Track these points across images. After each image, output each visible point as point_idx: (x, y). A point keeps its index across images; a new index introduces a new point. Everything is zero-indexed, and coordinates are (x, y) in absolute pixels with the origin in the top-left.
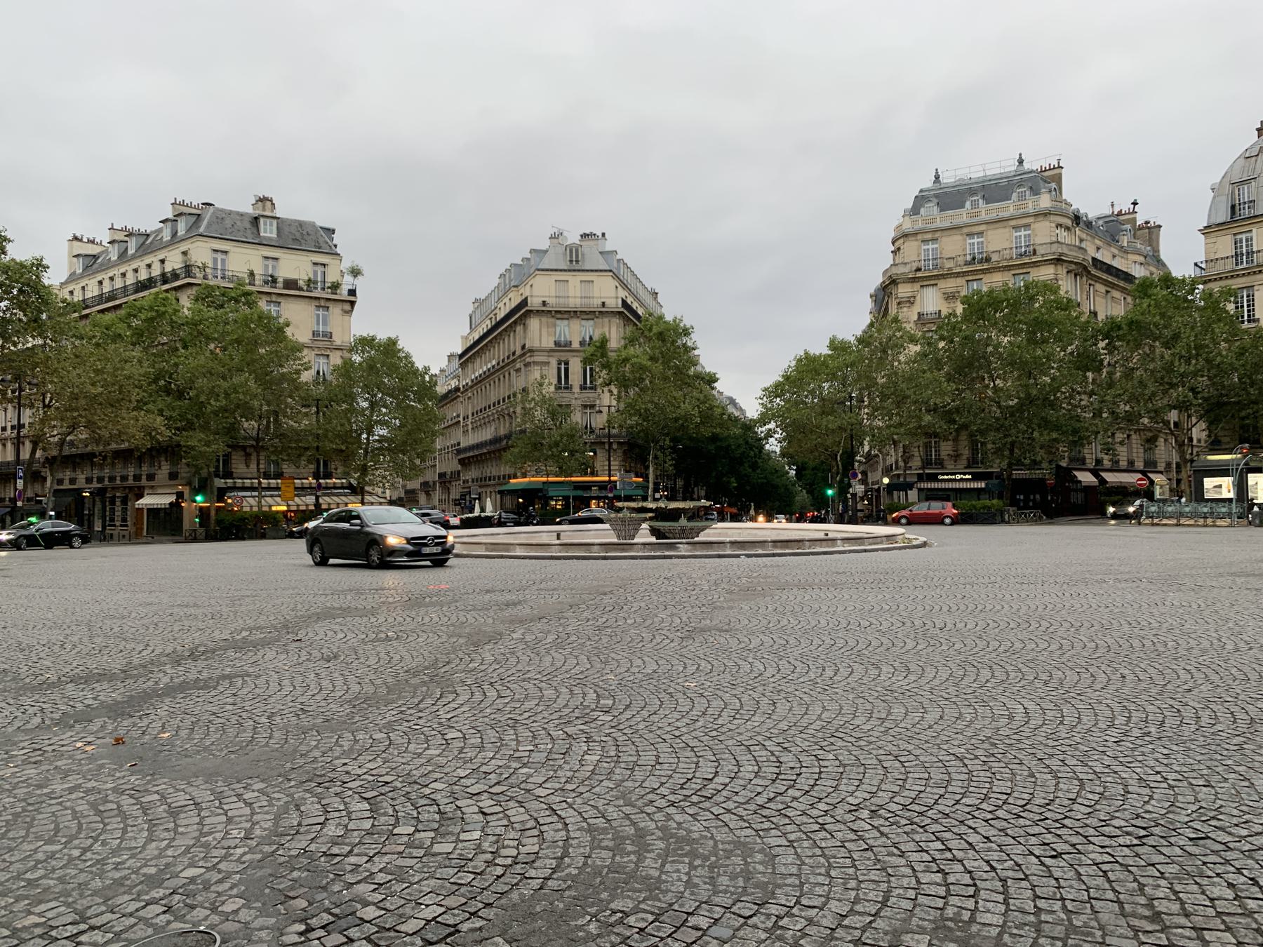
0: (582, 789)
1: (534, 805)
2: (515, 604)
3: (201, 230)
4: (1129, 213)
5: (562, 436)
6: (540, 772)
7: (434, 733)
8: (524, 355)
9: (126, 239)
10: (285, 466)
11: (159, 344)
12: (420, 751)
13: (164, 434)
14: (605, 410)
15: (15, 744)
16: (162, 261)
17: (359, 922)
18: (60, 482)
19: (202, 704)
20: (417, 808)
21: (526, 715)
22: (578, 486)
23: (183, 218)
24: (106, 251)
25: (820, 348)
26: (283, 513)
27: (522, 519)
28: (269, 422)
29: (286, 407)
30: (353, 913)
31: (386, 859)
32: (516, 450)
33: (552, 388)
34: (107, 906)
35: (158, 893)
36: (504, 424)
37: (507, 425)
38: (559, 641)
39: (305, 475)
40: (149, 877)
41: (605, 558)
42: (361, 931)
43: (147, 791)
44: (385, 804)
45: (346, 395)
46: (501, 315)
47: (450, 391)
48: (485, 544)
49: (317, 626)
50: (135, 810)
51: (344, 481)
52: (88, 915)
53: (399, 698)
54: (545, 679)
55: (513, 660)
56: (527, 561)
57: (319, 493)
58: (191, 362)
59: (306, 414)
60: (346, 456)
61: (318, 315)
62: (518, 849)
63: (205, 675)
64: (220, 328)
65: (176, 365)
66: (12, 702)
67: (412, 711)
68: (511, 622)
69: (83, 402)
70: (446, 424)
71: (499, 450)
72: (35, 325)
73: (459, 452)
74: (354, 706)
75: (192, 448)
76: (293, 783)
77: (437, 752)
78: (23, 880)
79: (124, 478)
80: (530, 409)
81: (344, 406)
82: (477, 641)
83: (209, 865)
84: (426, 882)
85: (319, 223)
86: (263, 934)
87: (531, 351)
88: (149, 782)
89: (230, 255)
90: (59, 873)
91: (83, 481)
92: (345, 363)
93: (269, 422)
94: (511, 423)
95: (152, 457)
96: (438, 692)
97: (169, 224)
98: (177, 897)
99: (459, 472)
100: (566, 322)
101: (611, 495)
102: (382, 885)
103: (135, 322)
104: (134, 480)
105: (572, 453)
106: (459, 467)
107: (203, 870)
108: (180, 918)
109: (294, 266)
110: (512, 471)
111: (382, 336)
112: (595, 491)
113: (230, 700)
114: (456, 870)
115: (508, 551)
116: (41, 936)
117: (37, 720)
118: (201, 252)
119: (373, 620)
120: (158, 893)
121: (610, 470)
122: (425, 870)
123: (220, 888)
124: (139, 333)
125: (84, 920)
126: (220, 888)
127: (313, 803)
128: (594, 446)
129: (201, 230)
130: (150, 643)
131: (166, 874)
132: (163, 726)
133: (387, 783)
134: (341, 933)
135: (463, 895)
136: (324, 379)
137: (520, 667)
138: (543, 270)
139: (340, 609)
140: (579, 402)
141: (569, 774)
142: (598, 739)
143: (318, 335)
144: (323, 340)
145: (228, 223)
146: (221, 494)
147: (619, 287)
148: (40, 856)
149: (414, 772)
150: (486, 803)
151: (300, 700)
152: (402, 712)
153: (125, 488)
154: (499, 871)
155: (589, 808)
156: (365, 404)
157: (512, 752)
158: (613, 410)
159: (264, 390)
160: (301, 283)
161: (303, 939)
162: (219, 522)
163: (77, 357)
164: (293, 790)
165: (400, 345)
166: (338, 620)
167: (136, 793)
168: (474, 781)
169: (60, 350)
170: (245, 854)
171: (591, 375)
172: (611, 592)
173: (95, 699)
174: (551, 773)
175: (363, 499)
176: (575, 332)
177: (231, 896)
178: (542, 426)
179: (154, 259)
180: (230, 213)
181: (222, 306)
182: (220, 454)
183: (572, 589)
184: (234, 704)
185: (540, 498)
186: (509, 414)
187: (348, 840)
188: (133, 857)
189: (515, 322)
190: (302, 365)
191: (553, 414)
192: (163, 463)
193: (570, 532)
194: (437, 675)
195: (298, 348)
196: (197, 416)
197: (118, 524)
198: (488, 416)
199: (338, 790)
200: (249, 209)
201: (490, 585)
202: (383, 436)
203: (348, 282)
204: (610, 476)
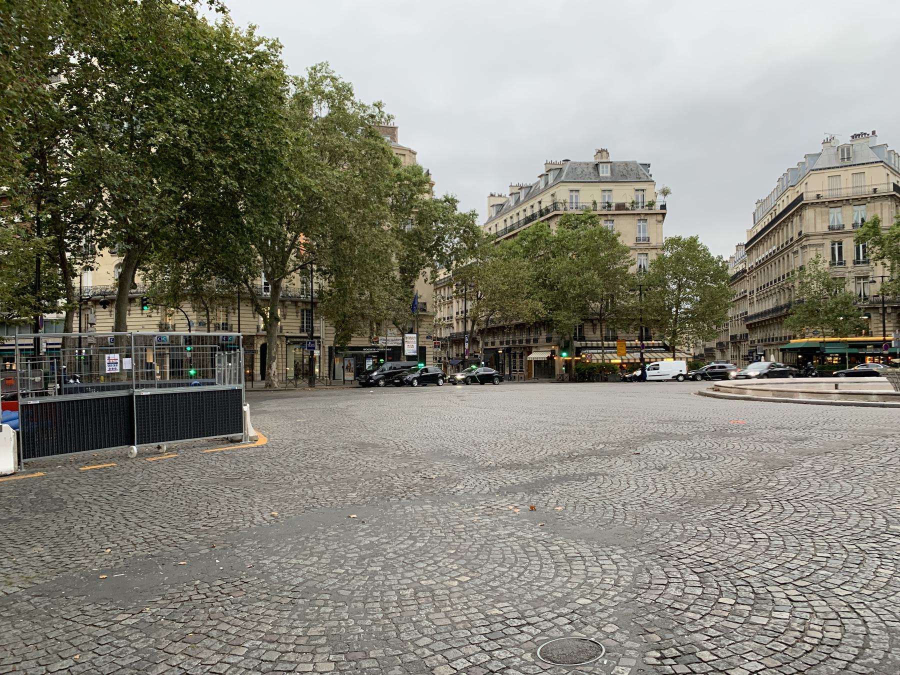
0: (877, 595)
1: (834, 601)
2: (802, 440)
3: (563, 178)
5: (837, 304)
6: (837, 576)
7: (744, 532)
8: (800, 239)
9: (519, 191)
10: (619, 332)
11: (539, 256)
12: (735, 544)
13: (543, 313)
14: (879, 280)
15: (477, 502)
16: (540, 202)
17: (698, 661)
18: (486, 344)
19: (580, 491)
20: (735, 586)
21: (821, 529)
22: (853, 345)
23: (552, 172)
24: (508, 201)
26: (621, 364)
27: (802, 372)
28: (607, 303)
29: (619, 292)
30: (694, 653)
31: (715, 619)
32: (795, 316)
33: (827, 265)
34: (535, 611)
35: (565, 610)
36: (784, 296)
37: (787, 296)
38: (846, 472)
39: (633, 338)
40: (558, 599)
41: (883, 406)
42: (701, 667)
43: (551, 543)
44: (710, 579)
45: (660, 281)
46: (780, 210)
47: (738, 273)
48: (772, 391)
49: (649, 445)
50: (546, 554)
51: (660, 342)
52: (526, 615)
53: (714, 503)
54: (835, 502)
55: (805, 484)
56: (810, 405)
57: (643, 351)
58: (558, 266)
59: (633, 296)
60: (661, 325)
61: (640, 226)
62: (822, 633)
63: (579, 472)
64: (575, 242)
65: (549, 268)
66: (473, 476)
67: (726, 514)
68: (801, 453)
69: (498, 295)
70: (736, 298)
71: (780, 317)
72: (472, 251)
73: (747, 319)
74: (682, 505)
75: (560, 322)
76: (643, 553)
77: (748, 547)
78: (489, 586)
79: (521, 341)
80: (807, 283)
81: (659, 289)
82: (773, 466)
83: (594, 599)
84: (746, 643)
85: (639, 161)
86: (632, 653)
87: (806, 236)
88: (552, 538)
89: (581, 192)
90: (507, 586)
91: (498, 343)
92: (659, 258)
93: (607, 303)
94: (790, 295)
95: (536, 328)
96: (745, 502)
97: (543, 177)
98: (576, 616)
99: (747, 335)
101: (886, 352)
102: (713, 637)
103: (525, 243)
105: (847, 318)
106: (747, 331)
107: (590, 601)
108: (579, 630)
109: (623, 194)
110: (792, 333)
111: (686, 236)
112: (870, 349)
113: (597, 490)
114: (772, 639)
115: (792, 397)
116: (501, 622)
117: (487, 489)
118: (563, 193)
119: (689, 443)
120: (565, 610)
121: (884, 331)
122: (746, 634)
123: (602, 615)
124: (527, 250)
125: (524, 618)
126: (602, 615)
127: (658, 569)
128: (868, 311)
129: (563, 178)
130: (544, 447)
131: (568, 599)
132: (557, 502)
133: (711, 564)
134: (686, 665)
135: (778, 659)
136: (645, 271)
137: (811, 490)
138: (817, 170)
139: (664, 433)
140: (853, 275)
141: (865, 581)
142: (890, 557)
143: (640, 240)
144: (643, 243)
145: (579, 171)
146: (578, 351)
147: (891, 175)
148: (496, 573)
149: (731, 559)
150: (792, 592)
151: (643, 495)
152: (717, 513)
154: (808, 647)
155: (886, 612)
156: (675, 287)
157: (811, 556)
158: (886, 279)
159: (604, 281)
160: (628, 205)
161: (659, 663)
162: (577, 370)
163: (494, 268)
164: (644, 558)
165: (700, 241)
166: (664, 442)
167: (547, 544)
168: (780, 574)
169: (485, 265)
170: (615, 596)
171: (864, 252)
172: (893, 435)
173: (517, 479)
174: (848, 578)
175: (674, 355)
176: (847, 217)
177: (609, 623)
178: (818, 297)
179: (534, 202)
180: (580, 164)
181: (576, 227)
182: (577, 325)
183: (854, 431)
184: (599, 493)
185: (818, 355)
186: (788, 288)
187: (685, 600)
188: (547, 584)
189: (792, 215)
190: (629, 262)
191: (828, 287)
192: (543, 332)
193: (847, 384)
194: (742, 489)
195: (626, 250)
196: (562, 301)
197: (518, 370)
198: (770, 290)
199: (676, 563)
200: (593, 160)
201: (779, 424)
202: (687, 309)
203: (660, 200)
204: (884, 335)
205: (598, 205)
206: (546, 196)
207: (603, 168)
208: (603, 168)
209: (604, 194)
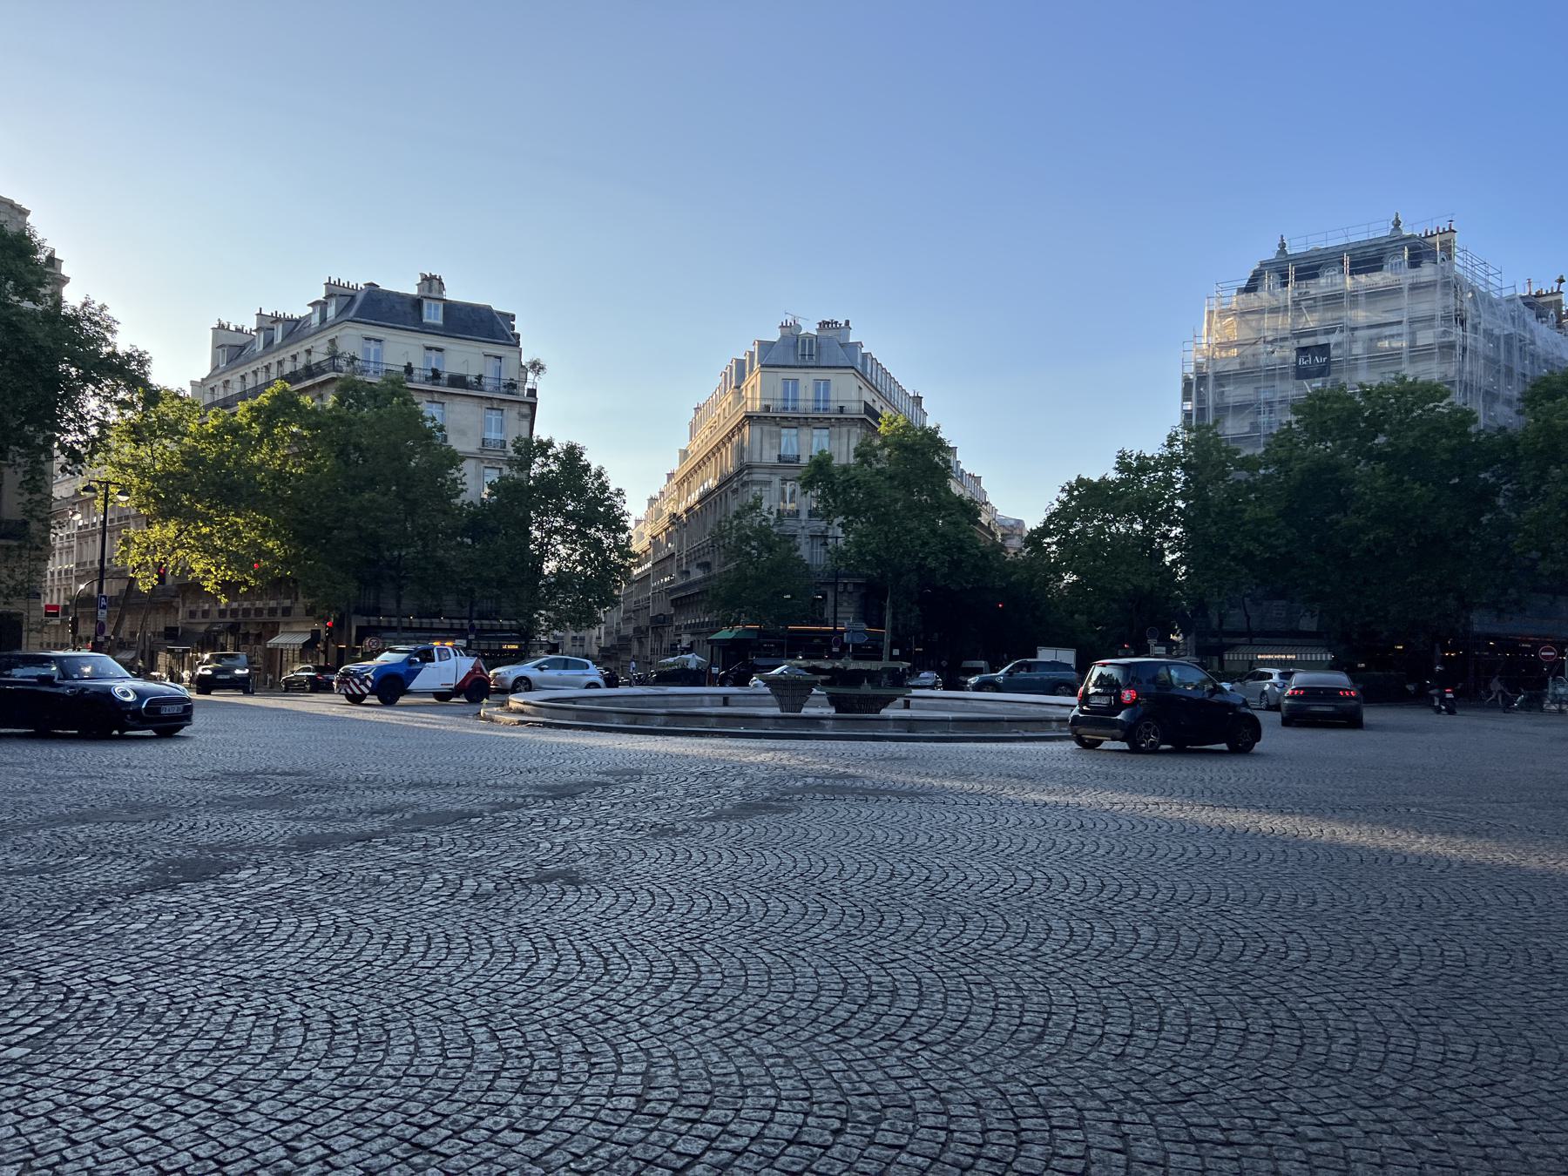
4: (1552, 294)
9: (271, 325)
16: (309, 352)
25: (1103, 469)
51: (514, 622)
87: (749, 467)
89: (385, 344)
100: (794, 431)
104: (256, 615)
140: (807, 532)
147: (864, 389)
153: (259, 623)
205: (416, 372)
206: (319, 343)
207: (429, 307)
208: (429, 307)
209: (368, 346)
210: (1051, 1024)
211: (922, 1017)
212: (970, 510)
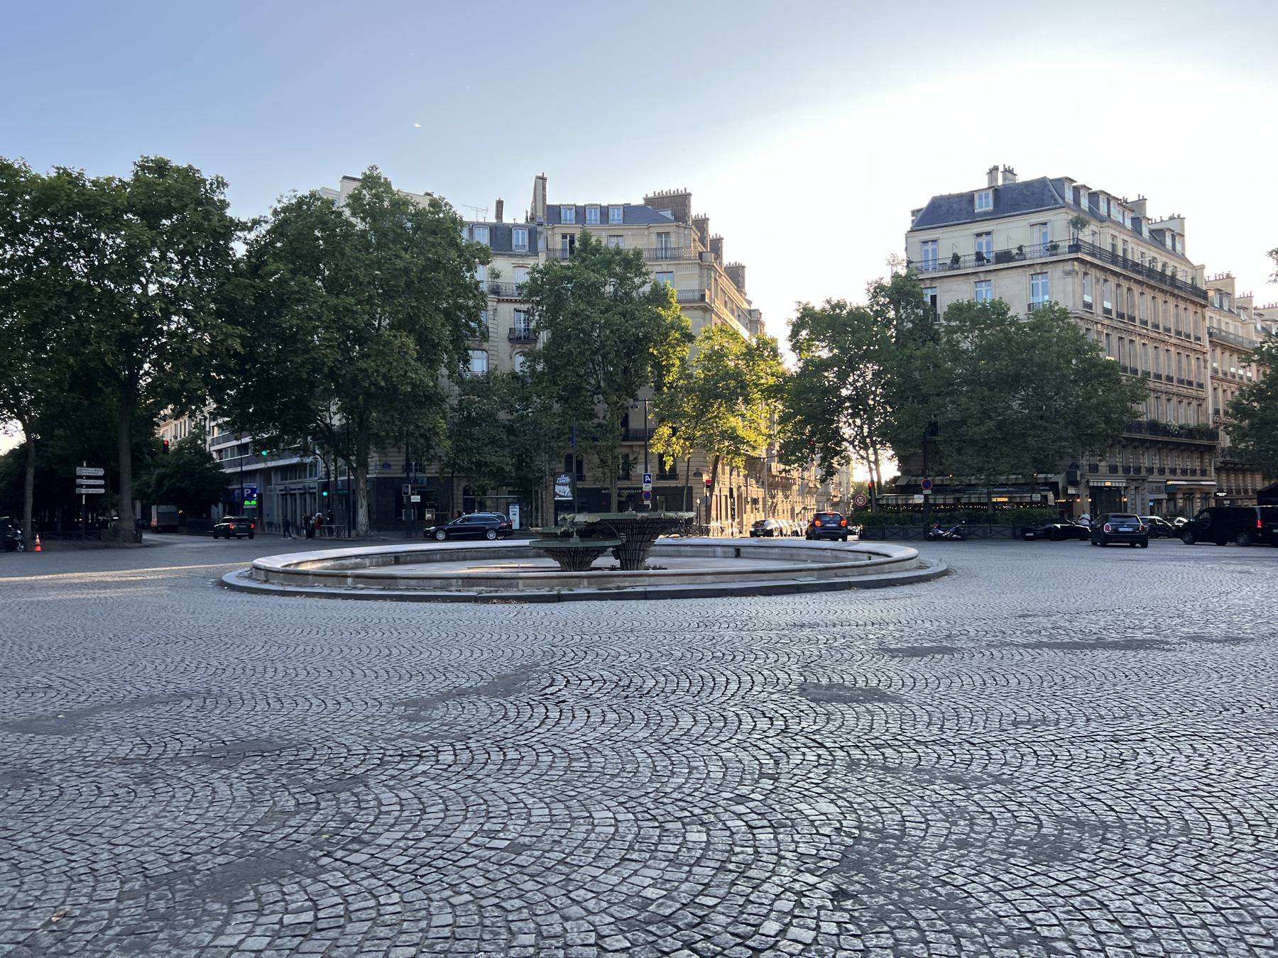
89: (994, 235)
160: (1014, 252)
210: (593, 836)
211: (1138, 845)
212: (22, 446)
